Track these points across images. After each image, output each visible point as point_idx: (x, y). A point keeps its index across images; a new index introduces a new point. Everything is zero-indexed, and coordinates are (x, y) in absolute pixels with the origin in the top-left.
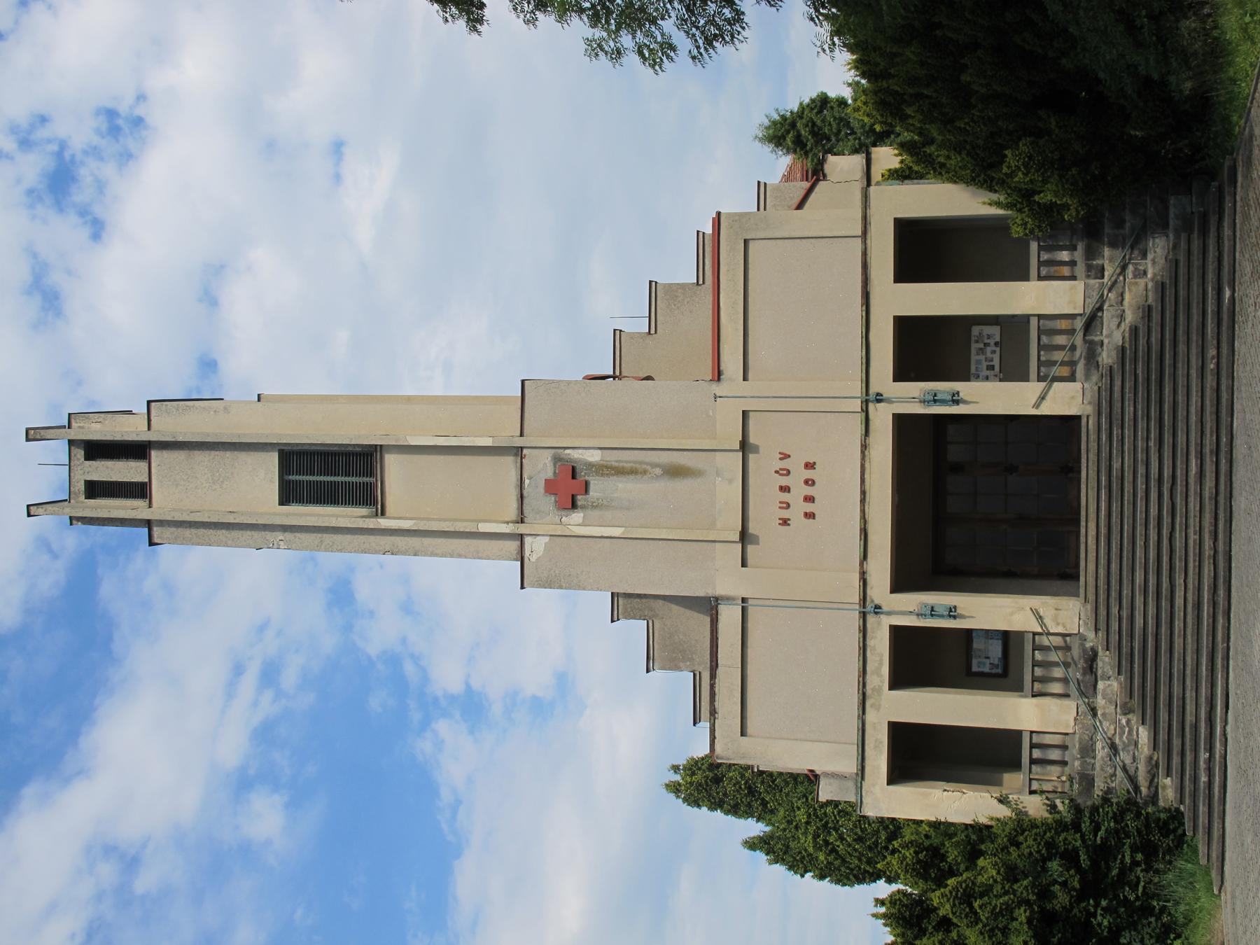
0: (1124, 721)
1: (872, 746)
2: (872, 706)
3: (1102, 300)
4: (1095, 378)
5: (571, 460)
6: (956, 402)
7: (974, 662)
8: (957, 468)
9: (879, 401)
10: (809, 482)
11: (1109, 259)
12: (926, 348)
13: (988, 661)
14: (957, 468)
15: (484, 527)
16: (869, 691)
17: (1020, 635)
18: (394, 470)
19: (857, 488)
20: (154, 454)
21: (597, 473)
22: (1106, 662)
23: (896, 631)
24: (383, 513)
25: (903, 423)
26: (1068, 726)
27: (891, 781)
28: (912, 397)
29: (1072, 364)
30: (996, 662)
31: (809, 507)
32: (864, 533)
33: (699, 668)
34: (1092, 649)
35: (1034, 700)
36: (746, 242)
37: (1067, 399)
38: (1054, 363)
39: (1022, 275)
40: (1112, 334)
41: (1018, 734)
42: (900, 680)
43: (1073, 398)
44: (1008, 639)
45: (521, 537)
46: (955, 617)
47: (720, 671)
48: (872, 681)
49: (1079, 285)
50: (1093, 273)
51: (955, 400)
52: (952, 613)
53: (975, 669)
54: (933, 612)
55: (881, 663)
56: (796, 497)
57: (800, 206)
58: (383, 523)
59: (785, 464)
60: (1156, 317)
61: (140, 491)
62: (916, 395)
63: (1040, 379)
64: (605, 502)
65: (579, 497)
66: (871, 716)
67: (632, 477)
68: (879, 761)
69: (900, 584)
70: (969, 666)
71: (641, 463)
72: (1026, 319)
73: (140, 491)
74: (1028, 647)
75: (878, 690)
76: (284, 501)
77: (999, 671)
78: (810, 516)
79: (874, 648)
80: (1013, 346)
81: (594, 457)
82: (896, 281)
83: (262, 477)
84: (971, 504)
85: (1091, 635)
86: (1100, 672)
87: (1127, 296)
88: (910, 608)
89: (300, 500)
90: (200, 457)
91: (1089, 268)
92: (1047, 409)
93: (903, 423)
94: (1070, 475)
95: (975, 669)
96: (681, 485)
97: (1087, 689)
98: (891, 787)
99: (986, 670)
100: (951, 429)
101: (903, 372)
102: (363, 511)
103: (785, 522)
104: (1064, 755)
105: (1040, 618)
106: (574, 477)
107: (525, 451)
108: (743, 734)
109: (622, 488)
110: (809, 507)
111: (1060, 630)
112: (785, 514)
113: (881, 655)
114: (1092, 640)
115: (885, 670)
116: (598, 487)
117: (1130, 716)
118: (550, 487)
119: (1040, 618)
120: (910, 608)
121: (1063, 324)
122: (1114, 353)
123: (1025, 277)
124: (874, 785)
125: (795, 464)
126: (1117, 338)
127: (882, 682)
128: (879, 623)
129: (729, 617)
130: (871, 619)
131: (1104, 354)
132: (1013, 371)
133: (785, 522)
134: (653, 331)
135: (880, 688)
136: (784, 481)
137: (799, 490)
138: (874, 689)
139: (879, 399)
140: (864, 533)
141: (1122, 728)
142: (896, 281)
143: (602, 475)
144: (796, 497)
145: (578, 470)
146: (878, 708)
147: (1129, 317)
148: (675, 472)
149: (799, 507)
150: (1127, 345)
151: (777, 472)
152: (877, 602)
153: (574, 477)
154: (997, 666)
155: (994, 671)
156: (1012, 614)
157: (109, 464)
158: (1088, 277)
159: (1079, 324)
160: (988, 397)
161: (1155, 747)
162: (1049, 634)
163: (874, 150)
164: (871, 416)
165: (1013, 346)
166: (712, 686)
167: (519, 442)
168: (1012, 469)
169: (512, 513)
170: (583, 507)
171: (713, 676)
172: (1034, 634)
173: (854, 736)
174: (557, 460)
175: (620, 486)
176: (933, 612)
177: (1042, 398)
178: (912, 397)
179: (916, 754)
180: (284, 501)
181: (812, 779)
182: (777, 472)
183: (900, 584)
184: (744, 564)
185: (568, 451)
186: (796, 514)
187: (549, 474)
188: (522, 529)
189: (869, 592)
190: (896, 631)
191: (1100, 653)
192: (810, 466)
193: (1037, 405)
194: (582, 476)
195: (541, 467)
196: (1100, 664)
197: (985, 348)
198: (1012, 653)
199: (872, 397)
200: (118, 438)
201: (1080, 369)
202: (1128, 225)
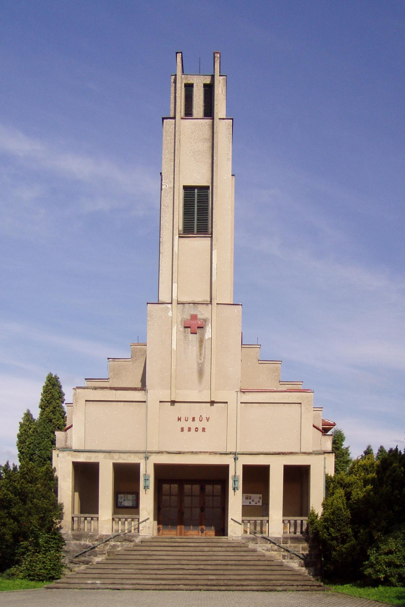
2: (106, 456)
4: (243, 541)
5: (205, 326)
6: (234, 489)
7: (122, 495)
8: (202, 489)
9: (235, 459)
11: (303, 548)
12: (256, 477)
14: (202, 489)
15: (175, 285)
16: (111, 454)
17: (138, 513)
18: (198, 244)
19: (196, 449)
20: (208, 121)
22: (126, 544)
24: (180, 237)
25: (226, 468)
27: (73, 463)
28: (236, 472)
31: (186, 430)
32: (180, 453)
33: (110, 380)
35: (111, 518)
36: (300, 403)
37: (236, 530)
39: (286, 513)
40: (261, 548)
41: (97, 513)
42: (77, 466)
43: (235, 533)
44: (136, 507)
45: (171, 303)
46: (145, 488)
47: (114, 391)
48: (116, 456)
50: (285, 540)
52: (146, 487)
53: (120, 496)
54: (146, 480)
55: (123, 459)
56: (190, 424)
57: (314, 426)
58: (176, 237)
59: (204, 420)
60: (270, 563)
61: (188, 113)
62: (237, 474)
63: (243, 521)
65: (189, 329)
66: (101, 455)
68: (82, 458)
70: (120, 493)
71: (204, 358)
72: (267, 515)
73: (188, 113)
74: (134, 516)
75: (112, 458)
76: (185, 188)
77: (119, 505)
78: (182, 430)
80: (257, 510)
81: (208, 335)
83: (199, 179)
84: (192, 494)
86: (124, 543)
87: (275, 553)
88: (147, 472)
89: (186, 196)
90: (208, 144)
91: (287, 538)
92: (230, 523)
93: (226, 468)
95: (120, 496)
96: (195, 376)
98: (71, 463)
99: (119, 500)
100: (218, 487)
101: (247, 469)
102: (181, 228)
103: (179, 419)
105: (145, 521)
106: (198, 327)
107: (210, 305)
108: (86, 401)
109: (194, 348)
110: (186, 430)
111: (141, 528)
112: (183, 419)
114: (137, 540)
115: (121, 461)
116: (193, 338)
117: (107, 554)
118: (194, 317)
119: (145, 521)
120: (147, 472)
122: (253, 548)
123: (284, 515)
124: (71, 456)
125: (204, 424)
126: (259, 549)
128: (141, 459)
129: (138, 396)
130: (142, 456)
131: (252, 544)
132: (247, 511)
133: (179, 419)
134: (260, 362)
135: (114, 459)
136: (197, 419)
137: (193, 425)
139: (235, 459)
140: (180, 453)
144: (190, 424)
145: (201, 329)
146: (105, 458)
147: (267, 553)
148: (201, 373)
149: (186, 425)
152: (150, 458)
154: (121, 504)
159: (264, 535)
160: (236, 501)
161: (98, 563)
162: (139, 524)
163: (334, 454)
164: (229, 456)
165: (257, 510)
166: (106, 388)
167: (214, 302)
168: (202, 509)
169: (182, 300)
170: (185, 332)
171: (111, 388)
172: (139, 519)
173: (88, 448)
174: (205, 320)
175: (195, 348)
176: (146, 480)
178: (236, 472)
179: (86, 475)
180: (185, 188)
181: (63, 427)
184: (160, 402)
185: (210, 325)
186: (183, 424)
187: (199, 316)
188: (175, 303)
189: (154, 454)
191: (132, 543)
192: (204, 430)
193: (232, 519)
194: (199, 331)
195: (203, 313)
197: (256, 499)
198: (127, 510)
200: (216, 103)
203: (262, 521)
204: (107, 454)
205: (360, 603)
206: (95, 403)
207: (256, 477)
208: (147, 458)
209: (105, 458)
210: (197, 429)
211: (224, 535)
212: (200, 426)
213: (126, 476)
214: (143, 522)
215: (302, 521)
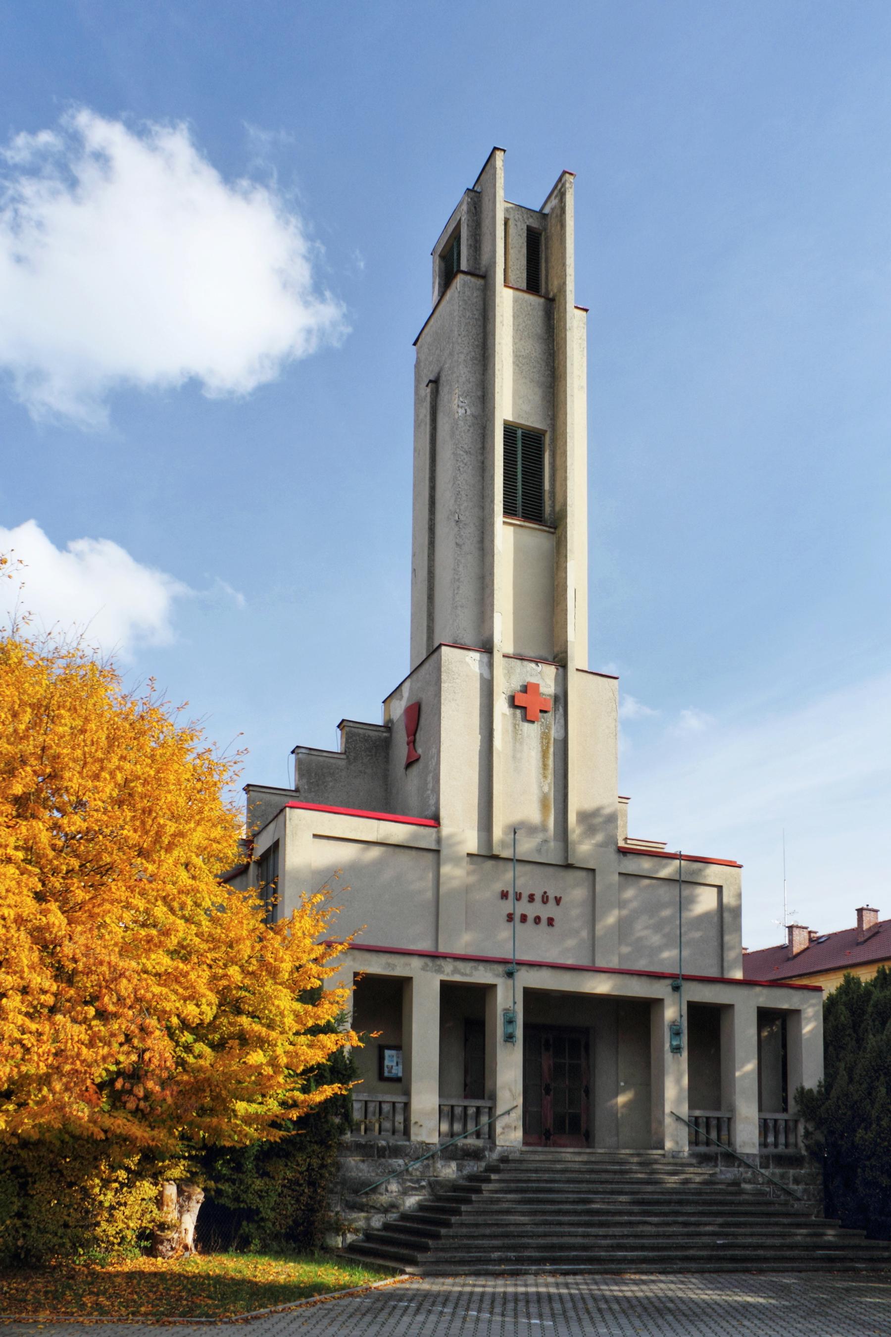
0: (424, 1183)
1: (390, 961)
2: (427, 965)
3: (748, 1166)
10: (537, 920)
13: (394, 1064)
21: (544, 733)
23: (491, 988)
26: (417, 1135)
29: (708, 1143)
30: (394, 1071)
34: (484, 1156)
38: (708, 1132)
42: (448, 990)
49: (755, 1151)
51: (676, 1050)
53: (387, 1053)
54: (510, 1021)
55: (463, 974)
59: (552, 901)
64: (519, 736)
66: (416, 963)
67: (541, 764)
68: (376, 966)
69: (530, 995)
75: (440, 970)
77: (386, 1074)
79: (476, 969)
82: (758, 1008)
85: (495, 1156)
86: (465, 1163)
88: (507, 999)
94: (544, 1137)
97: (449, 1152)
98: (494, 983)
104: (387, 1131)
105: (508, 1112)
106: (541, 711)
113: (470, 975)
115: (457, 978)
119: (508, 1112)
120: (507, 999)
121: (724, 1137)
123: (441, 1096)
124: (354, 960)
127: (448, 975)
130: (500, 969)
135: (443, 972)
136: (538, 898)
138: (440, 966)
141: (418, 1181)
142: (758, 1008)
143: (542, 738)
146: (424, 968)
150: (664, 1186)
151: (545, 893)
153: (541, 711)
154: (390, 1072)
155: (386, 1070)
156: (510, 1091)
157: (497, 255)
158: (761, 1157)
176: (510, 1021)
177: (678, 1119)
182: (545, 893)
183: (530, 995)
190: (491, 988)
192: (551, 922)
196: (472, 1163)
199: (679, 981)
201: (702, 1149)
202: (796, 1187)
203: (478, 1108)
204: (428, 961)
205: (433, 1318)
206: (332, 842)
207: (707, 1027)
208: (510, 975)
209: (424, 968)
210: (537, 920)
211: (588, 1147)
212: (545, 912)
213: (464, 1010)
214: (503, 1114)
215: (465, 1108)
